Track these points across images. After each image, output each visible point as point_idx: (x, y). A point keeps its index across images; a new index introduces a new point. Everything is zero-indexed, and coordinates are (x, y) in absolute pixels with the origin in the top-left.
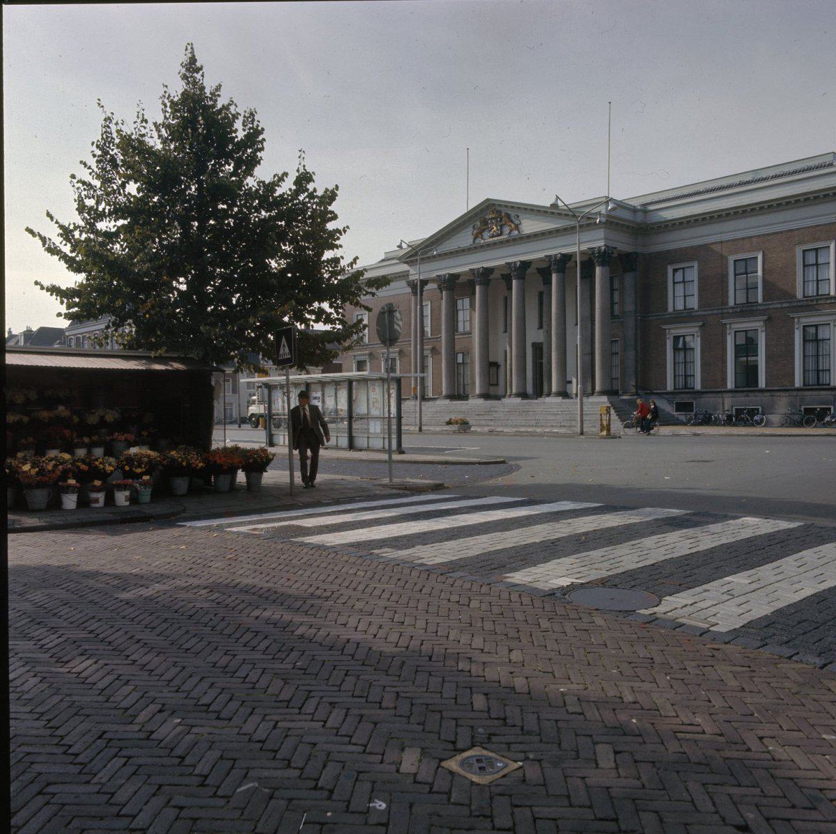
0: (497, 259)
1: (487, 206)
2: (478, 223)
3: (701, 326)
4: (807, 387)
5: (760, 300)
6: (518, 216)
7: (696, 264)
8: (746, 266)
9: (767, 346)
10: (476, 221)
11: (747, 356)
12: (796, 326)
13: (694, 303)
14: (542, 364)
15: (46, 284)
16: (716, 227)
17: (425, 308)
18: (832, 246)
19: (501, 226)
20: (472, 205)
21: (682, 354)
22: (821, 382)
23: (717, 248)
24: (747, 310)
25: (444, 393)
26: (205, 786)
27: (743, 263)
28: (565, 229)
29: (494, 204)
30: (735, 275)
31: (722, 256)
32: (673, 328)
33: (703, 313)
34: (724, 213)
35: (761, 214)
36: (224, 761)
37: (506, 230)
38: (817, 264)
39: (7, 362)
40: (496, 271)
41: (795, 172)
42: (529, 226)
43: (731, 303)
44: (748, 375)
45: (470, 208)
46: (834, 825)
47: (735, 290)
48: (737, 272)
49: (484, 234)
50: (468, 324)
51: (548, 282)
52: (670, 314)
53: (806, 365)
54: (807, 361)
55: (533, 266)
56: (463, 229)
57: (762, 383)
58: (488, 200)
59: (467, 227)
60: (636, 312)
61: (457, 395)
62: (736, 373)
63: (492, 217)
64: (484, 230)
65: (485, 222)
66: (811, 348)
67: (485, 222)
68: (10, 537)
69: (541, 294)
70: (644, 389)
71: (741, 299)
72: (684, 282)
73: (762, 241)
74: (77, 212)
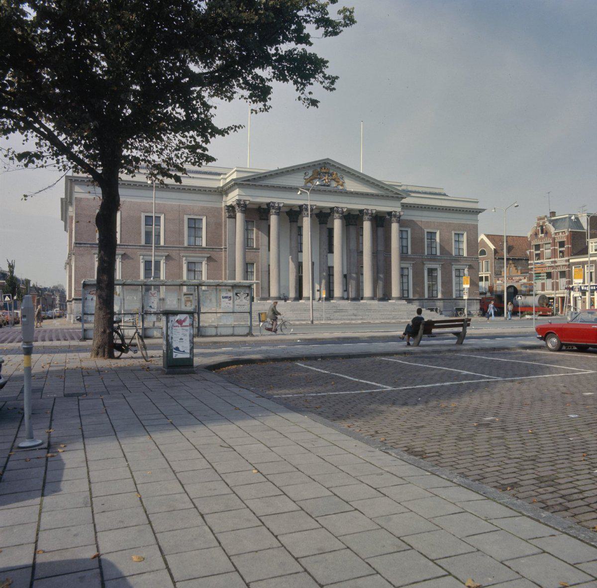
5: (438, 254)
8: (432, 235)
9: (442, 277)
15: (231, 132)
16: (426, 213)
18: (465, 234)
23: (419, 223)
24: (433, 258)
26: (448, 572)
27: (193, 221)
28: (378, 195)
31: (421, 228)
34: (192, 189)
35: (128, 188)
36: (296, 562)
41: (425, 193)
42: (351, 185)
46: (596, 491)
58: (328, 159)
63: (323, 171)
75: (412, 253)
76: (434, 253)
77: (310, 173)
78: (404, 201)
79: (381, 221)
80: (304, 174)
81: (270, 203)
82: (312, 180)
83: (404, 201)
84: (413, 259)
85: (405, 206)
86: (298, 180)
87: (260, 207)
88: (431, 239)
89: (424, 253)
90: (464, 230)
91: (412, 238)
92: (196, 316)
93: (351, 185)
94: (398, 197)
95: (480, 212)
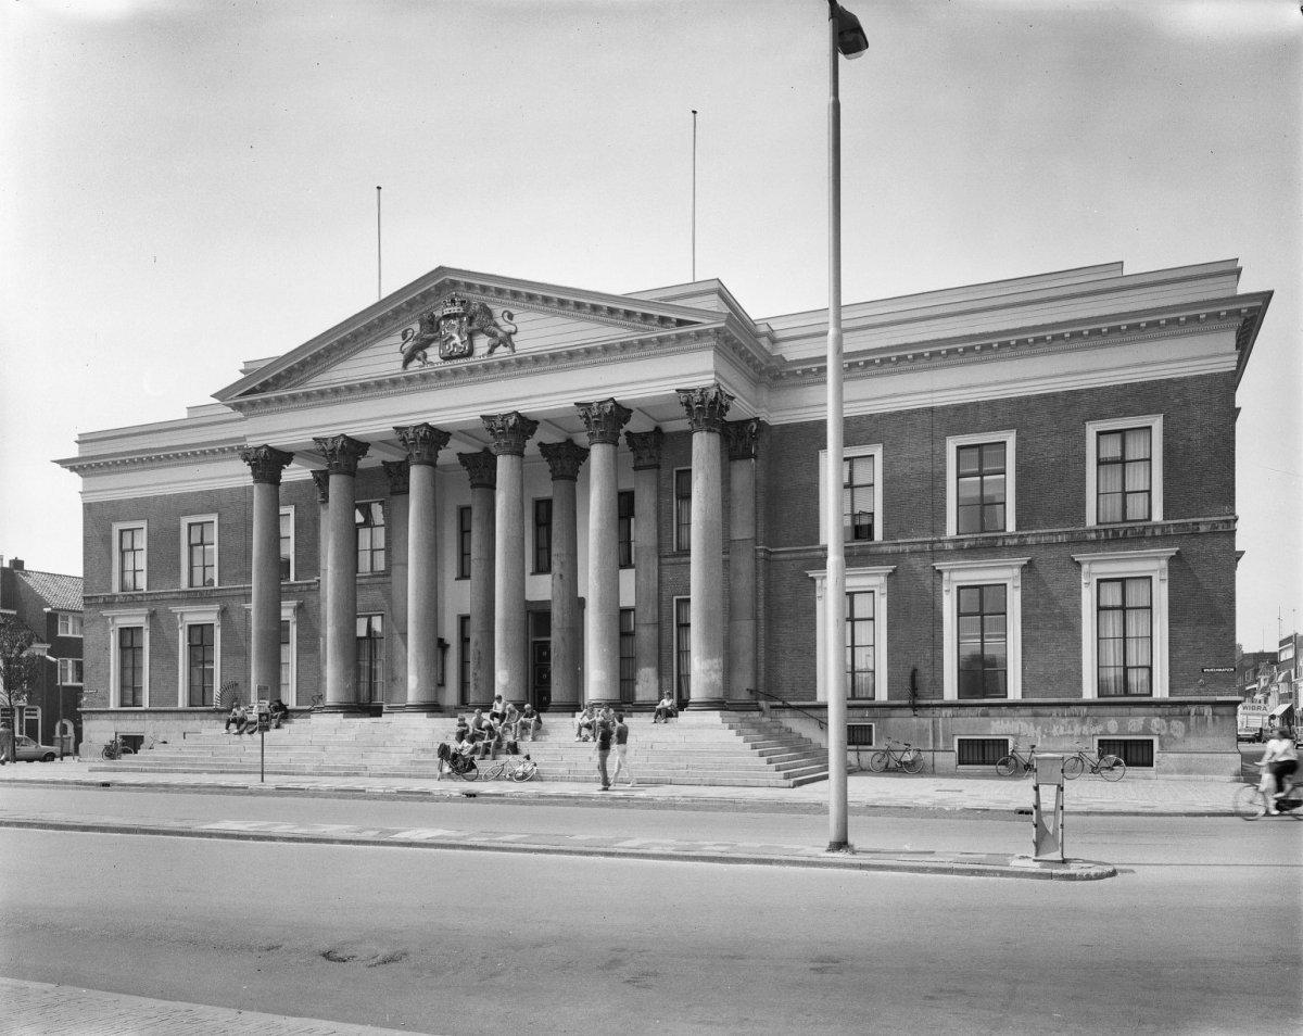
0: (458, 406)
1: (440, 288)
2: (416, 327)
3: (890, 575)
6: (511, 316)
7: (878, 451)
10: (411, 321)
14: (545, 646)
17: (283, 521)
19: (471, 335)
20: (394, 283)
25: (331, 697)
29: (455, 284)
33: (890, 549)
37: (482, 344)
39: (383, 569)
40: (452, 443)
43: (1091, 521)
44: (981, 677)
45: (383, 297)
47: (1098, 494)
49: (429, 351)
50: (380, 558)
53: (1102, 657)
54: (1102, 647)
55: (543, 435)
56: (378, 339)
57: (1014, 693)
58: (441, 270)
59: (388, 335)
60: (756, 540)
61: (363, 705)
63: (445, 313)
64: (428, 343)
65: (432, 324)
67: (432, 324)
68: (81, 575)
69: (464, 513)
70: (769, 697)
74: (19, 559)
86: (385, 359)
87: (658, 430)
89: (1082, 519)
90: (1148, 411)
93: (534, 332)
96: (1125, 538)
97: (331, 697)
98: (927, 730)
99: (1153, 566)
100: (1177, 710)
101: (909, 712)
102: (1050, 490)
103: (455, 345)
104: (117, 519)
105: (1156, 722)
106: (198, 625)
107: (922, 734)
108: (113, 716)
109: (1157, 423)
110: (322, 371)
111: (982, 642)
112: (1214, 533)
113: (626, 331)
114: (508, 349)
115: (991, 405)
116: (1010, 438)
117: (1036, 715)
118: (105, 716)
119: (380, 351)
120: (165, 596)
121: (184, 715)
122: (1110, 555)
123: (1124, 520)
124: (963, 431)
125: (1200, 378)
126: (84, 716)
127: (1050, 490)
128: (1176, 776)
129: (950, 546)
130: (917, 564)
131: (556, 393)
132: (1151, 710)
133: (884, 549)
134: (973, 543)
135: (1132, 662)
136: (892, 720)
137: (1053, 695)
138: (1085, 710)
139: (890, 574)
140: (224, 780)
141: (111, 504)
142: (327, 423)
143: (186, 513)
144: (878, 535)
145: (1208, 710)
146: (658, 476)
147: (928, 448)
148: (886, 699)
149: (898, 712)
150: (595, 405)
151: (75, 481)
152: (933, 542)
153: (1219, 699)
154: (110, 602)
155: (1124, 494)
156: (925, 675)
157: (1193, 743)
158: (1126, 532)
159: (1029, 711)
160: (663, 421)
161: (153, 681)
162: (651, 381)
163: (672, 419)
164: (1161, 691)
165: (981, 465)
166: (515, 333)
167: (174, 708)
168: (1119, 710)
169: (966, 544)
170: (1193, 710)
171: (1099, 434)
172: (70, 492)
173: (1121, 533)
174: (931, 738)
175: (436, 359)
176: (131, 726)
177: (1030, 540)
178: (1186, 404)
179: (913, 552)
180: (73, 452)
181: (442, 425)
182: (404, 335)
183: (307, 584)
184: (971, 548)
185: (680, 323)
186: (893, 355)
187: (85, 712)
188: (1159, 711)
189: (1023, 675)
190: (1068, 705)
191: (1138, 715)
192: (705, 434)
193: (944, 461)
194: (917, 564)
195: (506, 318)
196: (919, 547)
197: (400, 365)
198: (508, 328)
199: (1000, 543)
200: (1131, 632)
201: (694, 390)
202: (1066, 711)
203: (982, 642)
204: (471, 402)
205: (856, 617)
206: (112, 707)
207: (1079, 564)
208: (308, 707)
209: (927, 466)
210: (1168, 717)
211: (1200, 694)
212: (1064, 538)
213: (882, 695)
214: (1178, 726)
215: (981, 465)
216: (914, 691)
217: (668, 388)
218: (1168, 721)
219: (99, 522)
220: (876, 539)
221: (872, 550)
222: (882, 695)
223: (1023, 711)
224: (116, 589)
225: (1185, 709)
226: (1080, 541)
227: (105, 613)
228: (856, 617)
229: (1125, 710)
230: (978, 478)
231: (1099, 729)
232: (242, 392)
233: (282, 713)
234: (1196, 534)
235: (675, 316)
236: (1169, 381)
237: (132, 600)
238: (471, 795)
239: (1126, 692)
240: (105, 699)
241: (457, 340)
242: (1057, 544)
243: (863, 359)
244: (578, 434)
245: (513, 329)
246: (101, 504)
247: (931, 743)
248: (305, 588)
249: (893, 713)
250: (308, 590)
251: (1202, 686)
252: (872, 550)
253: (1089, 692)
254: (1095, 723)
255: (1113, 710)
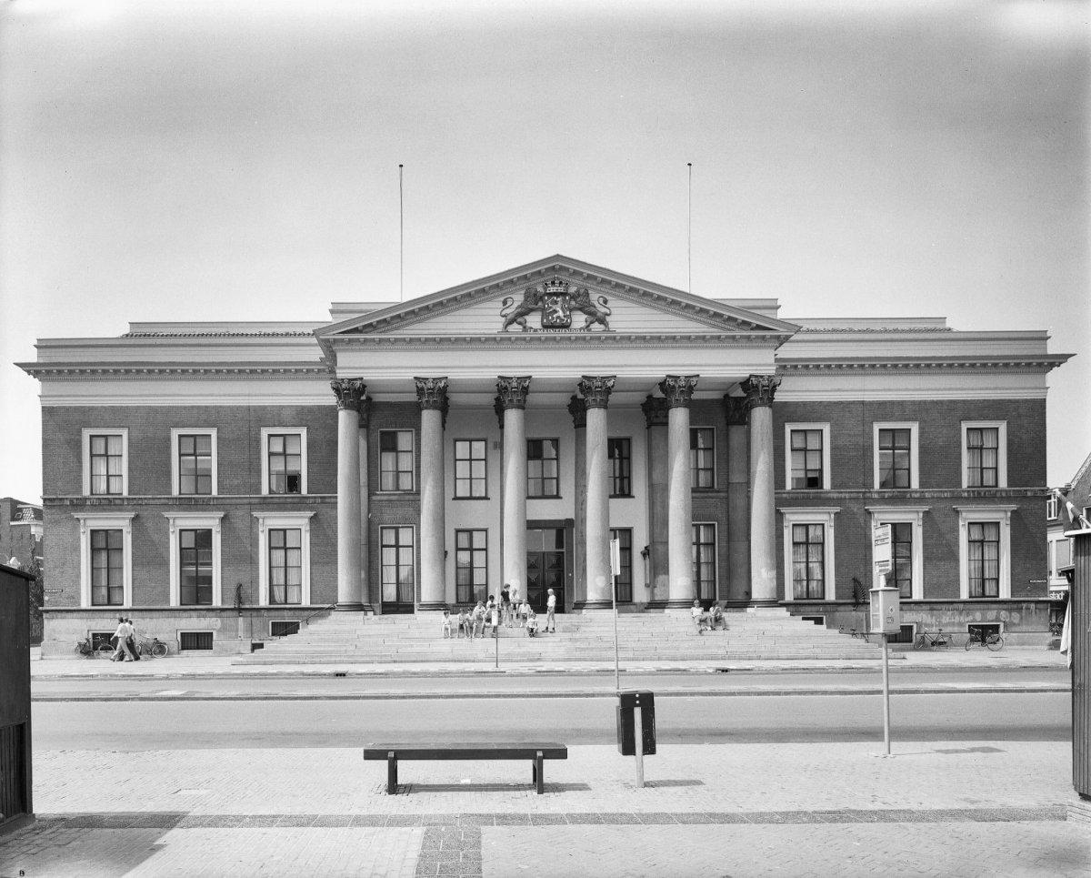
0: (555, 366)
3: (133, 519)
4: (975, 599)
6: (605, 302)
11: (197, 565)
12: (171, 530)
13: (122, 487)
21: (104, 555)
22: (987, 594)
25: (343, 596)
27: (102, 441)
30: (180, 455)
32: (269, 517)
33: (835, 495)
38: (106, 455)
47: (180, 475)
48: (182, 452)
51: (581, 424)
52: (788, 493)
58: (558, 257)
62: (181, 586)
63: (555, 293)
66: (279, 556)
71: (188, 488)
72: (106, 455)
73: (918, 410)
75: (834, 486)
76: (989, 478)
77: (518, 298)
78: (787, 351)
79: (724, 412)
80: (501, 305)
81: (748, 379)
82: (522, 314)
83: (787, 351)
84: (838, 502)
85: (786, 367)
86: (486, 318)
87: (727, 396)
88: (894, 448)
89: (959, 484)
90: (997, 418)
91: (833, 449)
92: (853, 601)
93: (625, 317)
94: (763, 338)
95: (1052, 366)
96: (985, 497)
97: (343, 596)
98: (862, 620)
99: (1000, 515)
100: (1015, 606)
101: (235, 613)
102: (940, 461)
103: (558, 317)
104: (89, 426)
105: (1003, 614)
106: (103, 530)
107: (859, 622)
108: (84, 614)
109: (1003, 427)
110: (448, 318)
111: (807, 559)
112: (1035, 497)
113: (716, 330)
114: (602, 326)
115: (901, 404)
116: (915, 428)
117: (931, 610)
118: (75, 614)
119: (480, 312)
120: (151, 502)
121: (177, 613)
122: (981, 507)
123: (108, 493)
124: (884, 419)
125: (1026, 400)
126: (45, 615)
127: (940, 461)
128: (1017, 647)
129: (876, 496)
130: (855, 507)
131: (391, 368)
132: (1001, 606)
133: (831, 495)
134: (891, 495)
135: (987, 576)
136: (838, 614)
137: (241, 604)
138: (961, 606)
139: (312, 517)
140: (681, 665)
141: (170, 409)
142: (593, 364)
143: (177, 426)
144: (827, 484)
145: (1032, 606)
146: (368, 432)
147: (861, 428)
148: (792, 599)
149: (842, 608)
150: (682, 378)
151: (35, 385)
152: (864, 493)
153: (1041, 599)
154: (80, 504)
155: (982, 469)
156: (246, 591)
157: (1024, 628)
158: (985, 493)
159: (928, 607)
160: (373, 393)
161: (137, 584)
162: (724, 365)
163: (536, 392)
164: (1005, 593)
165: (894, 443)
166: (608, 315)
167: (166, 607)
168: (982, 606)
169: (886, 496)
170: (1024, 605)
171: (270, 436)
172: (29, 397)
173: (983, 494)
174: (865, 624)
175: (538, 325)
176: (195, 624)
177: (927, 495)
178: (1019, 416)
179: (850, 499)
180: (32, 356)
181: (371, 380)
182: (505, 303)
183: (321, 497)
184: (890, 498)
185: (759, 327)
186: (305, 368)
187: (47, 611)
188: (1005, 606)
189: (133, 588)
190: (952, 603)
191: (994, 609)
192: (767, 408)
193: (872, 438)
194: (855, 507)
195: (601, 302)
196: (855, 495)
197: (500, 326)
198: (604, 310)
199: (908, 496)
200: (986, 557)
201: (762, 377)
202: (951, 607)
203: (807, 559)
204: (529, 364)
205: (474, 547)
206: (126, 606)
207: (958, 512)
208: (327, 606)
209: (861, 441)
210: (1010, 611)
211: (1027, 596)
212: (949, 495)
213: (831, 596)
214: (1016, 617)
215: (894, 443)
216: (239, 599)
217: (409, 375)
218: (1010, 613)
219: (64, 434)
220: (825, 487)
221: (822, 495)
222: (831, 596)
223: (924, 607)
224: (86, 492)
225: (1020, 606)
226: (957, 498)
227: (76, 515)
228: (474, 547)
229: (985, 606)
230: (194, 458)
231: (971, 618)
232: (346, 329)
233: (658, 605)
234: (1025, 497)
235: (755, 322)
236: (1010, 401)
237: (109, 503)
238: (725, 671)
239: (984, 595)
240: (75, 597)
241: (561, 313)
242: (946, 498)
243: (124, 368)
244: (454, 394)
245: (608, 312)
246: (67, 409)
247: (865, 628)
248: (311, 501)
249: (839, 608)
250: (322, 503)
251: (1030, 591)
252: (822, 495)
253: (964, 595)
254: (968, 615)
255: (978, 606)
